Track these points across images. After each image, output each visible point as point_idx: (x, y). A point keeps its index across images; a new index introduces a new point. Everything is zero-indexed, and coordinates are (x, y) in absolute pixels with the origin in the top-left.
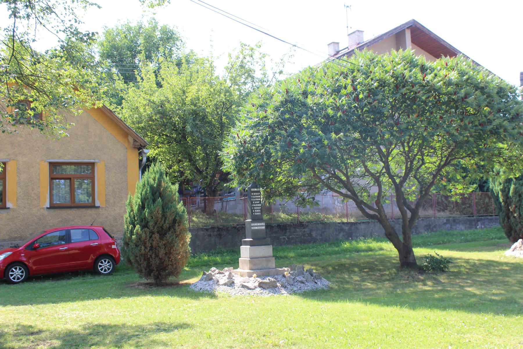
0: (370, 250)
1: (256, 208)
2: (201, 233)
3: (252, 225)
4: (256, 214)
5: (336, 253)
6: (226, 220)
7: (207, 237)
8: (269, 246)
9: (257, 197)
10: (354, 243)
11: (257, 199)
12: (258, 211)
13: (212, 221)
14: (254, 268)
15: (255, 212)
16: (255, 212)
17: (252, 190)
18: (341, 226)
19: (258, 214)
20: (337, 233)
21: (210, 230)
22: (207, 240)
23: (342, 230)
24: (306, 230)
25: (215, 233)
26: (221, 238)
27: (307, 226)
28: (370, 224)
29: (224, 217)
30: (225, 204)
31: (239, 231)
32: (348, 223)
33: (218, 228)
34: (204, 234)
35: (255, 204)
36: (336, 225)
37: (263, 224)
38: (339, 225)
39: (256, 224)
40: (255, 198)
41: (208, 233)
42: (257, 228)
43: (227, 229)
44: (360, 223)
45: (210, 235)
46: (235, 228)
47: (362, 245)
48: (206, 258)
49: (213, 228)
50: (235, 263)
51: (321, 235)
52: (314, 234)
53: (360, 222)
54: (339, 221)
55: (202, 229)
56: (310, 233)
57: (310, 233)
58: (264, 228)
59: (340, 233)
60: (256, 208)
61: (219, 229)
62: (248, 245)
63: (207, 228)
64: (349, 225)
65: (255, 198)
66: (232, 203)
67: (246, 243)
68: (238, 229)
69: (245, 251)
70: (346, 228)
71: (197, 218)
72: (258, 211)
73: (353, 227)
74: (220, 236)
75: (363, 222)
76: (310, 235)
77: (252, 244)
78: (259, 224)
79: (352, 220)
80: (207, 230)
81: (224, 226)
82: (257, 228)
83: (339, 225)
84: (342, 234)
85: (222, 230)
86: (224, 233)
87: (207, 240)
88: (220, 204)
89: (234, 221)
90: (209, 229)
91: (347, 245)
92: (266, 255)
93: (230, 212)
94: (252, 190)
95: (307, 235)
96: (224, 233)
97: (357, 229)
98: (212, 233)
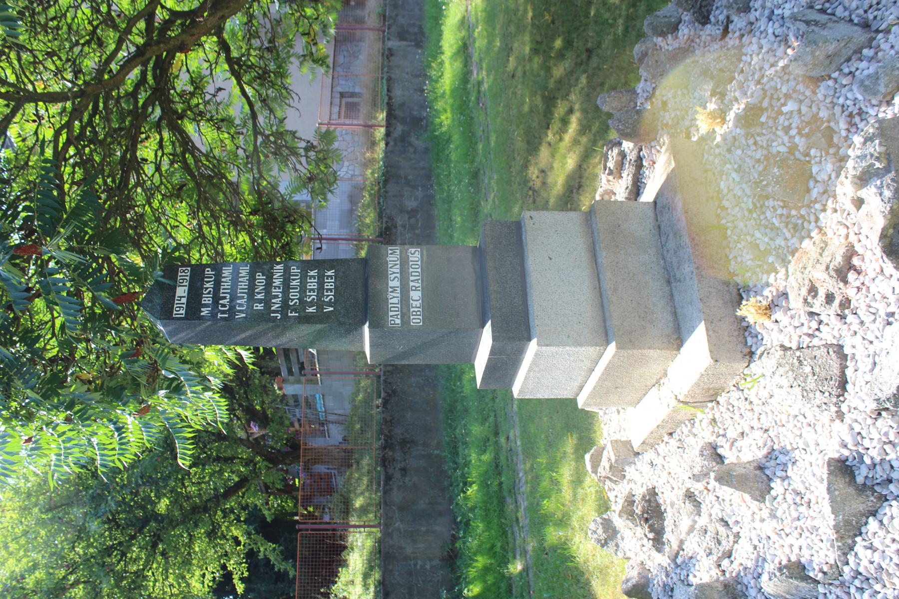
0: (464, 49)
1: (294, 295)
2: (396, 496)
3: (394, 319)
4: (330, 296)
5: (470, 139)
6: (365, 421)
7: (407, 480)
8: (528, 225)
9: (226, 284)
10: (439, 105)
11: (243, 284)
12: (312, 284)
13: (366, 461)
14: (663, 317)
15: (320, 304)
16: (320, 304)
17: (180, 311)
18: (395, 140)
19: (329, 284)
20: (412, 150)
21: (390, 471)
22: (415, 479)
23: (404, 139)
24: (399, 223)
25: (398, 455)
26: (412, 442)
27: (391, 218)
28: (393, 76)
29: (358, 426)
30: (331, 418)
31: (394, 392)
32: (389, 126)
33: (384, 448)
34: (399, 488)
35: (267, 302)
36: (392, 152)
37: (393, 256)
38: (392, 143)
39: (394, 299)
40: (216, 298)
41: (397, 475)
42: (416, 295)
43: (389, 422)
44: (390, 98)
45: (404, 470)
46: (386, 403)
47: (447, 74)
48: (472, 490)
49: (384, 462)
50: (571, 421)
51: (415, 187)
52: (411, 204)
53: (387, 98)
54: (382, 145)
55: (385, 493)
56: (408, 212)
57: (408, 212)
58: (415, 255)
59: (410, 144)
60: (294, 295)
61: (388, 445)
62: (519, 353)
63: (382, 477)
64: (394, 121)
65: (216, 298)
66: (330, 404)
67: (503, 365)
68: (389, 395)
69: (539, 373)
70: (399, 129)
71: (357, 496)
72: (312, 284)
73: (398, 113)
74: (406, 443)
75: (388, 90)
76: (412, 213)
77: (515, 331)
78: (394, 283)
79: (382, 116)
80: (388, 478)
81: (381, 432)
82: (416, 295)
83: (392, 143)
84: (413, 139)
85: (391, 437)
86: (398, 431)
87: (415, 479)
88: (331, 426)
89: (367, 402)
90: (386, 473)
91: (446, 119)
92: (579, 244)
93: (348, 407)
94: (180, 311)
95: (413, 221)
96: (398, 431)
97: (402, 105)
98: (398, 466)
